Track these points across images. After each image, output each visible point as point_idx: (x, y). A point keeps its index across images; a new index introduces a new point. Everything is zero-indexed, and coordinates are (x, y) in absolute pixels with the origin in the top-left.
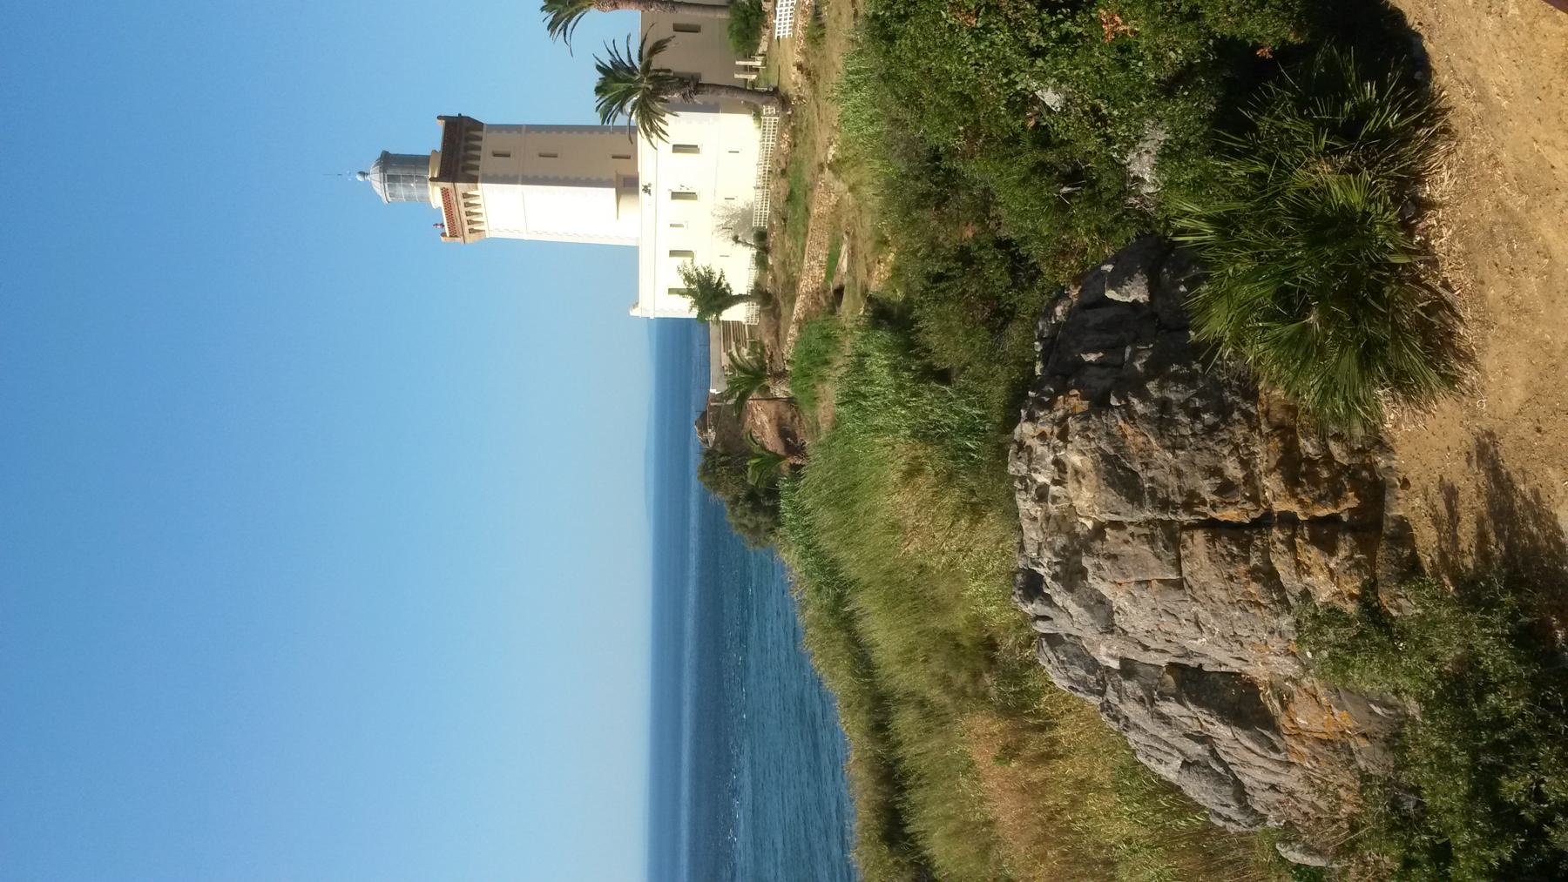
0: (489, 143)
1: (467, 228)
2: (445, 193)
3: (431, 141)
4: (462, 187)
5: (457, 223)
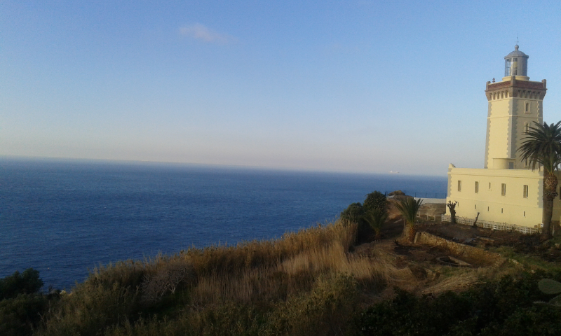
0: (534, 102)
1: (493, 92)
2: (508, 83)
3: (534, 76)
4: (511, 90)
5: (494, 90)
